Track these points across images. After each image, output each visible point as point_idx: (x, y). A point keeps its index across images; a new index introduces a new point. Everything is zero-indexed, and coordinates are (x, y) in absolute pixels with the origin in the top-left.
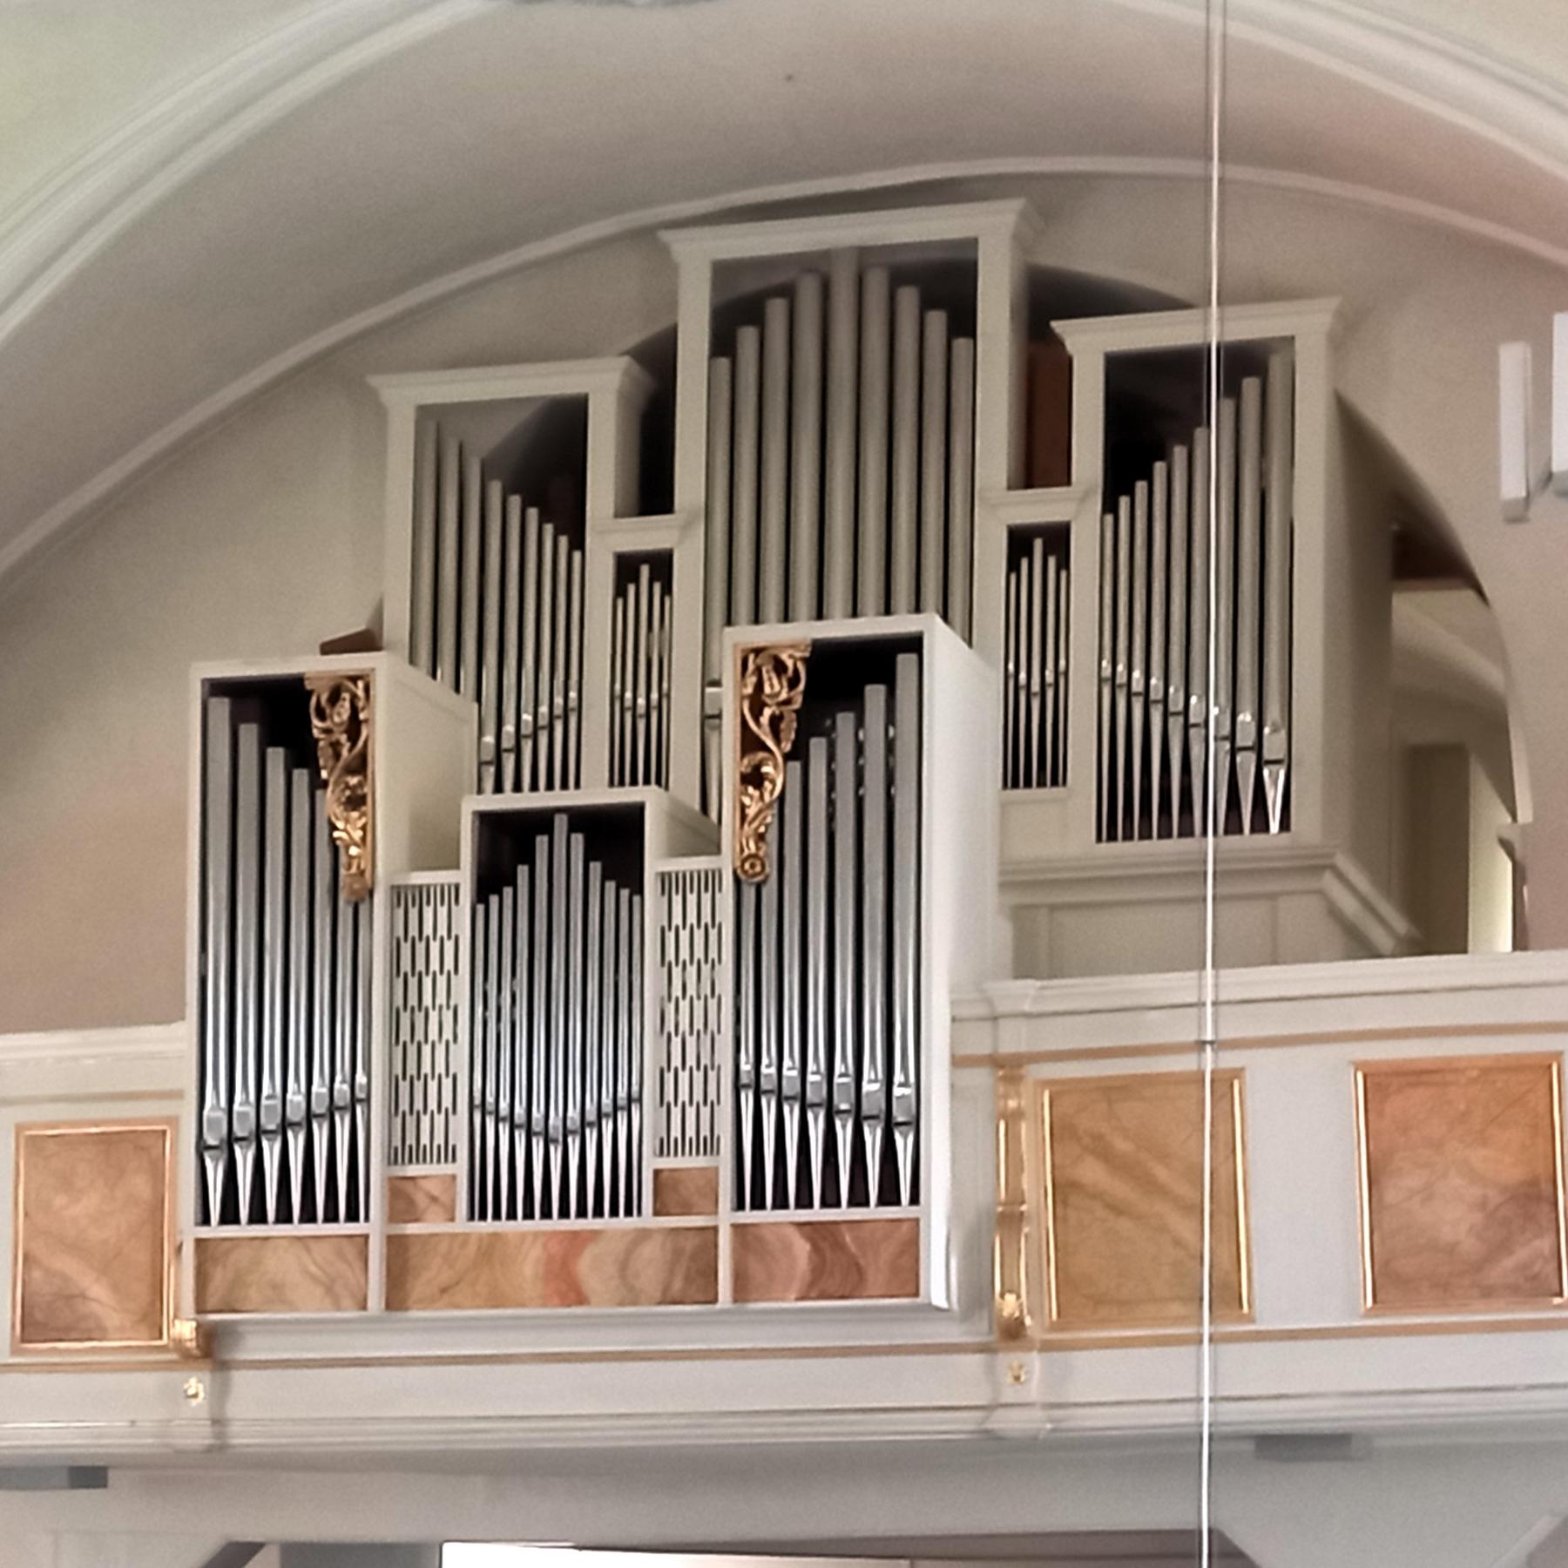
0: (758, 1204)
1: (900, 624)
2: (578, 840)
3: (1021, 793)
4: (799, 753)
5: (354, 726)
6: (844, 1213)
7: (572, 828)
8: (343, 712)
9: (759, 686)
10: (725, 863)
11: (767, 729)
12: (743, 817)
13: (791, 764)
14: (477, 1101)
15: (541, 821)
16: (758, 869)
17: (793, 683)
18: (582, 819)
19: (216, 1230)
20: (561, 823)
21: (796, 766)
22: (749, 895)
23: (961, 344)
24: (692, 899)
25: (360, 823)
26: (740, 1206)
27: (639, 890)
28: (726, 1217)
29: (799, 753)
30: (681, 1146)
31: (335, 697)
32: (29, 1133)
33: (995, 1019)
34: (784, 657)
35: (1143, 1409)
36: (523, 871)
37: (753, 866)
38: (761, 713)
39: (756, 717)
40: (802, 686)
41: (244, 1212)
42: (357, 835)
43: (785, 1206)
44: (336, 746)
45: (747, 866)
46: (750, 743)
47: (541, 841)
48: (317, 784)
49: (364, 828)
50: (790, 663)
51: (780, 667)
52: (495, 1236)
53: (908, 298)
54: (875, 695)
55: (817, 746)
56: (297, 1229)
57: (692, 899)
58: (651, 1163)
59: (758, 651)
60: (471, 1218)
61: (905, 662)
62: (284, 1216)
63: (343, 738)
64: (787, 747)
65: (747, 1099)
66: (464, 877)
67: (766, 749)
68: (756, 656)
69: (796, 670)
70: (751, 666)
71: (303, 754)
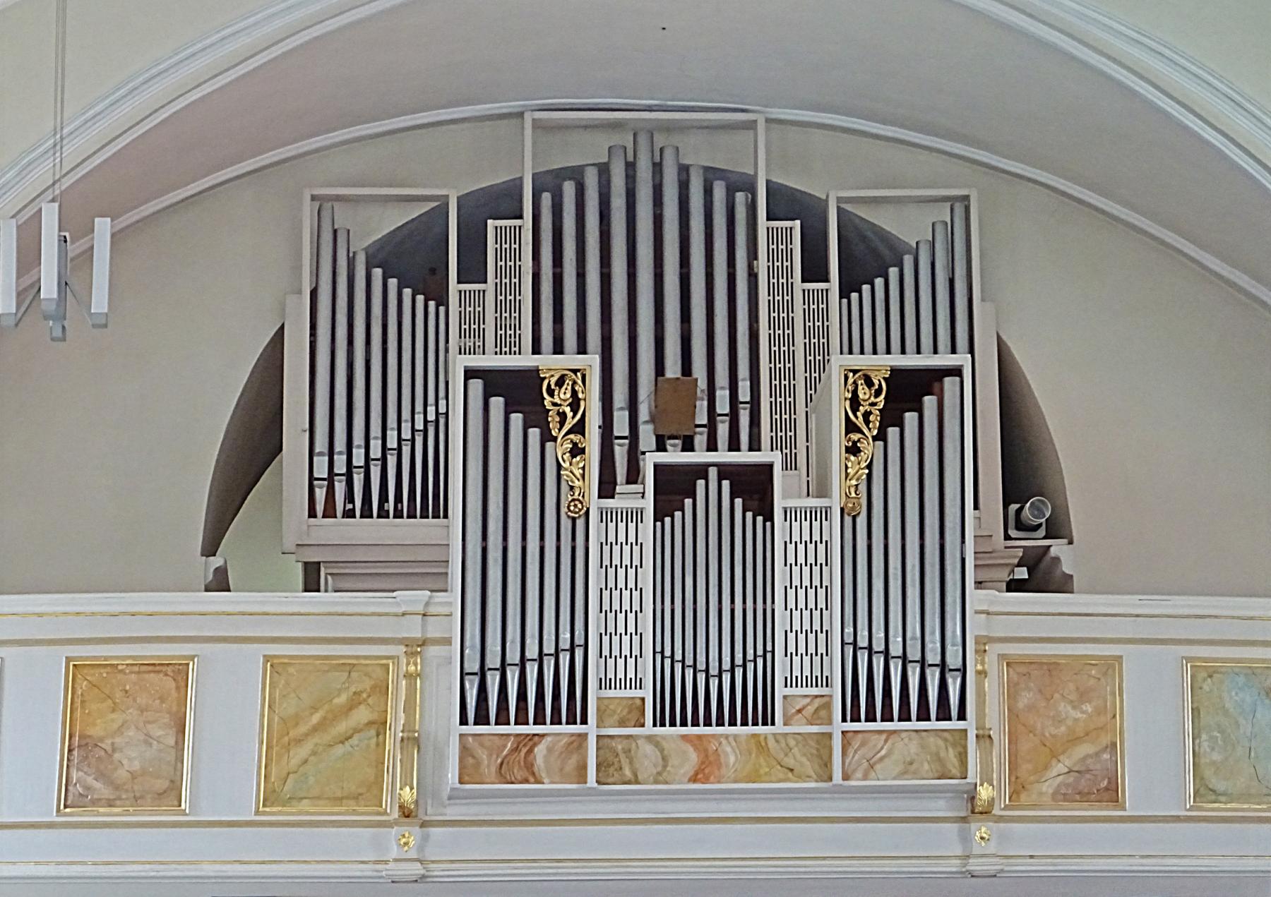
0: (856, 719)
1: (944, 360)
2: (726, 484)
3: (789, 472)
4: (881, 436)
5: (575, 405)
6: (714, 730)
7: (720, 478)
8: (564, 394)
9: (855, 392)
10: (836, 503)
11: (861, 418)
12: (847, 475)
13: (878, 443)
14: (658, 649)
15: (701, 471)
16: (580, 506)
17: (878, 393)
18: (725, 471)
19: (471, 729)
20: (713, 473)
21: (881, 444)
22: (848, 520)
23: (657, 159)
24: (622, 526)
25: (581, 465)
26: (844, 720)
27: (769, 517)
28: (838, 726)
29: (881, 436)
30: (626, 683)
31: (560, 383)
32: (391, 664)
33: (424, 615)
34: (872, 375)
35: (274, 866)
36: (688, 502)
37: (575, 506)
38: (858, 410)
39: (855, 411)
40: (883, 396)
41: (954, 712)
42: (578, 472)
43: (686, 725)
44: (563, 416)
45: (572, 508)
46: (851, 427)
47: (701, 483)
48: (547, 437)
49: (583, 468)
50: (876, 382)
51: (869, 383)
52: (754, 736)
54: (929, 402)
55: (893, 432)
56: (914, 725)
57: (622, 526)
58: (780, 691)
59: (855, 372)
60: (655, 725)
61: (949, 383)
62: (904, 716)
63: (568, 410)
64: (875, 432)
65: (849, 651)
67: (863, 433)
68: (854, 375)
69: (880, 385)
70: (851, 381)
71: (537, 417)
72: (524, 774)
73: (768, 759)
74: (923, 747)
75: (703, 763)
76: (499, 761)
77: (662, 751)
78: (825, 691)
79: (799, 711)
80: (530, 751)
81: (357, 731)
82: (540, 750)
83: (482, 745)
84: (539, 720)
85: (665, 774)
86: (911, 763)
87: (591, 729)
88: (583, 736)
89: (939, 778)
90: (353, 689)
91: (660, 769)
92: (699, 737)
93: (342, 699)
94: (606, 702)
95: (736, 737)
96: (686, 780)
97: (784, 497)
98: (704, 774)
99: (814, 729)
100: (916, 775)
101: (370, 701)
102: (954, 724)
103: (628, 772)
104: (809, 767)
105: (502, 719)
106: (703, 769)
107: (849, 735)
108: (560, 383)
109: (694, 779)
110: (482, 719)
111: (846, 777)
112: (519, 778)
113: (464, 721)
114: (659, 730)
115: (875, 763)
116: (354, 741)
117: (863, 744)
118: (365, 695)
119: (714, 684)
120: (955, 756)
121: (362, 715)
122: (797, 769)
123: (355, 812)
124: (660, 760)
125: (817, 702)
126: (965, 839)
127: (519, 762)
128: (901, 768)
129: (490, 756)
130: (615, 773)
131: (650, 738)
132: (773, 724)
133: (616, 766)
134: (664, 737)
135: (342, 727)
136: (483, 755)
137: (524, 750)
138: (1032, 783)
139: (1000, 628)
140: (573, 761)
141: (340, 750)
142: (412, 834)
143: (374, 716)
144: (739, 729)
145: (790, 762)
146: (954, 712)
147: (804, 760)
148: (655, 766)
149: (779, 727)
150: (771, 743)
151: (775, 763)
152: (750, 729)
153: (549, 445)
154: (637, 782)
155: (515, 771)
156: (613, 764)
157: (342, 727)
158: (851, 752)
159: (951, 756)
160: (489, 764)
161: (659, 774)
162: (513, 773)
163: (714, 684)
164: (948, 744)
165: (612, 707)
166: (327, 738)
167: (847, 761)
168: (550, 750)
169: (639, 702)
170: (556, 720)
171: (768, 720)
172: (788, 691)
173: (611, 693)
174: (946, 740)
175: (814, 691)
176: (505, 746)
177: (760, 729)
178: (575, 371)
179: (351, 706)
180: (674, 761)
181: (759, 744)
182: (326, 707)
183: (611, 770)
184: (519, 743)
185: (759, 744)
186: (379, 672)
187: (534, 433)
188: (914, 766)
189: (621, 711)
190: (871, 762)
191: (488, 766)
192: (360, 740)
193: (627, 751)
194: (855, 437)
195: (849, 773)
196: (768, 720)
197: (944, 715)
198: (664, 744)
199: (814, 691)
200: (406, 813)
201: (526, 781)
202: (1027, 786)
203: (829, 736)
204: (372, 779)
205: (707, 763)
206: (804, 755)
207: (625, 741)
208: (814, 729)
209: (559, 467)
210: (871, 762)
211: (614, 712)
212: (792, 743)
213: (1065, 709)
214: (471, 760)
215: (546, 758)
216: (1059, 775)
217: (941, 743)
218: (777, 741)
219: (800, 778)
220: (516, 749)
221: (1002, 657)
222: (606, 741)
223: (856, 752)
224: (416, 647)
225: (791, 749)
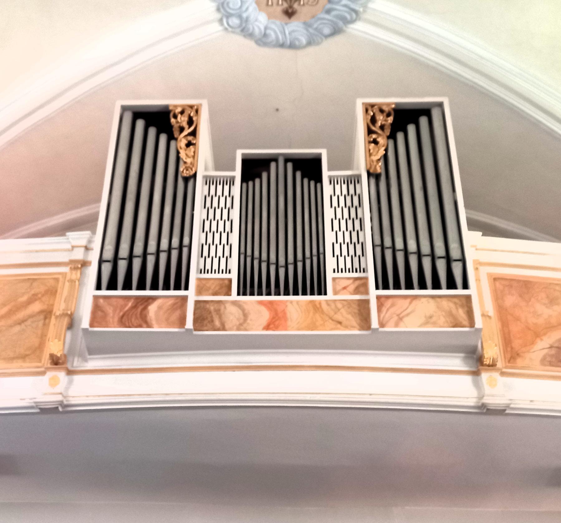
8: (183, 120)
19: (104, 292)
27: (319, 179)
28: (373, 293)
46: (370, 132)
52: (312, 302)
53: (290, 166)
60: (239, 294)
66: (237, 173)
72: (140, 321)
73: (322, 315)
74: (438, 307)
75: (273, 318)
76: (121, 314)
77: (243, 310)
78: (362, 275)
79: (345, 288)
80: (145, 308)
81: (31, 316)
82: (153, 308)
83: (110, 304)
84: (154, 287)
85: (245, 325)
86: (431, 317)
87: (191, 294)
88: (184, 299)
89: (454, 327)
90: (33, 292)
91: (241, 321)
92: (271, 302)
93: (24, 298)
94: (204, 282)
95: (298, 302)
96: (262, 327)
97: (330, 169)
98: (275, 325)
99: (357, 297)
100: (435, 324)
101: (44, 299)
102: (460, 292)
103: (217, 323)
104: (353, 321)
105: (127, 286)
106: (274, 322)
107: (383, 299)
108: (182, 113)
109: (267, 328)
110: (112, 285)
111: (382, 325)
112: (135, 324)
113: (99, 287)
114: (242, 298)
115: (403, 317)
116: (29, 322)
117: (393, 305)
118: (40, 296)
119: (282, 271)
120: (464, 313)
121: (36, 307)
122: (345, 322)
123: (21, 367)
124: (242, 316)
125: (358, 283)
126: (478, 385)
127: (136, 314)
128: (423, 320)
129: (115, 311)
130: (208, 324)
131: (234, 303)
132: (325, 294)
133: (209, 319)
134: (245, 302)
135: (21, 315)
136: (110, 310)
137: (140, 308)
138: (524, 352)
139: (484, 257)
140: (178, 313)
141: (17, 329)
142: (61, 375)
143: (44, 307)
144: (300, 298)
145: (338, 317)
146: (459, 280)
147: (350, 317)
148: (238, 319)
149: (330, 295)
150: (324, 306)
151: (327, 318)
152: (309, 298)
153: (173, 143)
154: (224, 329)
155: (133, 320)
156: (207, 318)
157: (21, 315)
158: (384, 310)
159: (461, 314)
160: (112, 314)
161: (241, 324)
162: (131, 321)
163: (282, 271)
164: (458, 306)
165: (208, 285)
166: (10, 321)
167: (382, 316)
168: (160, 308)
169: (226, 282)
170: (167, 287)
171: (322, 291)
172: (336, 275)
173: (206, 276)
174: (455, 303)
175: (355, 275)
176: (126, 305)
177: (316, 298)
178: (191, 107)
179: (30, 302)
180: (252, 316)
181: (316, 307)
182: (13, 304)
183: (206, 322)
184: (138, 303)
185: (316, 307)
186: (52, 282)
187: (163, 138)
188: (434, 319)
189: (214, 286)
190: (401, 316)
191: (113, 317)
192: (32, 322)
193: (218, 311)
194: (374, 136)
195: (384, 323)
196: (322, 291)
197: (451, 285)
198: (246, 307)
199: (355, 275)
200: (56, 362)
201: (140, 326)
202: (521, 354)
203: (367, 302)
204: (37, 345)
205: (277, 318)
206: (350, 313)
207: (216, 305)
208: (357, 297)
209: (178, 159)
210: (401, 316)
211: (210, 288)
212: (339, 305)
213: (540, 308)
214: (100, 313)
215: (157, 313)
216: (544, 349)
217: (452, 305)
218: (328, 305)
219: (346, 327)
220: (134, 307)
221: (489, 275)
222: (202, 305)
223: (388, 310)
224: (85, 264)
225: (339, 310)
